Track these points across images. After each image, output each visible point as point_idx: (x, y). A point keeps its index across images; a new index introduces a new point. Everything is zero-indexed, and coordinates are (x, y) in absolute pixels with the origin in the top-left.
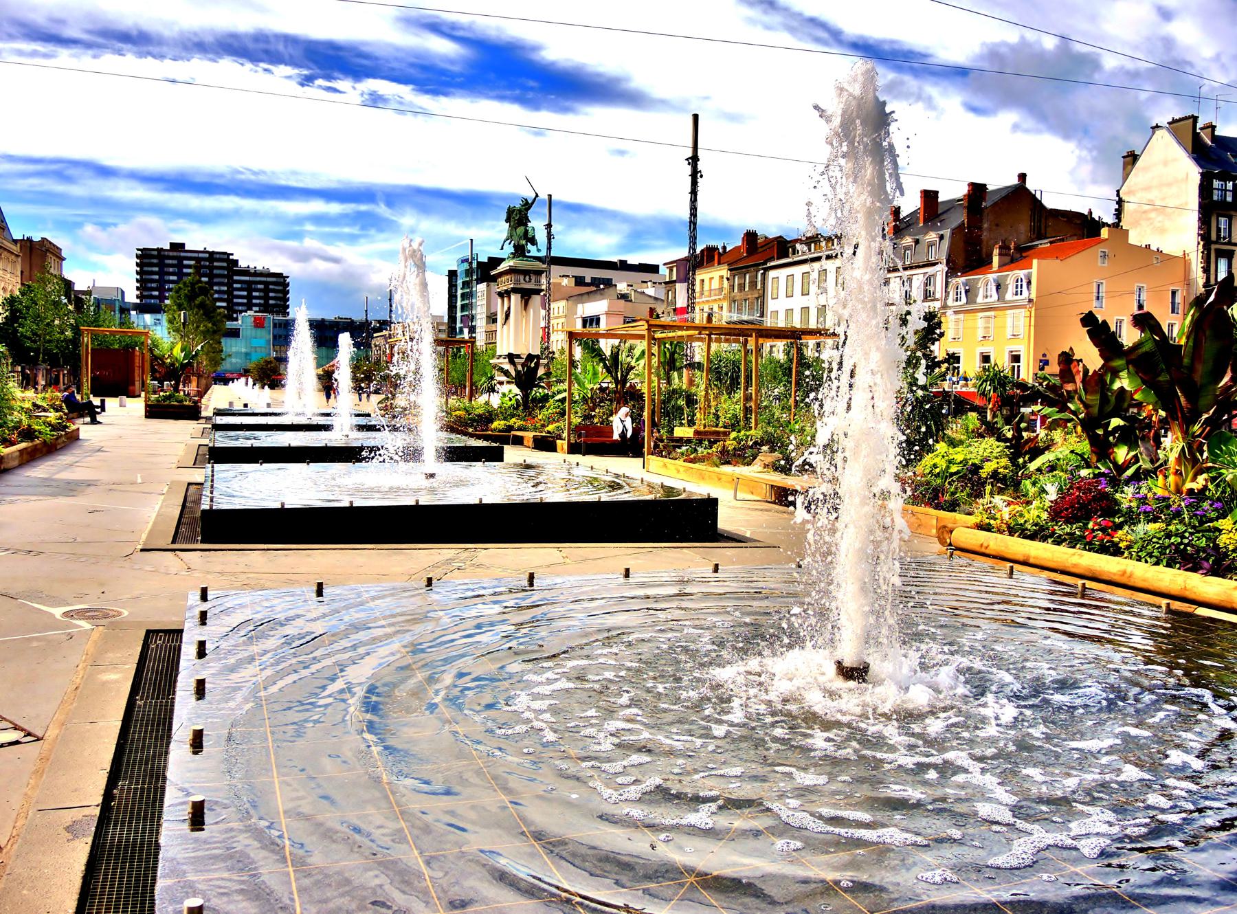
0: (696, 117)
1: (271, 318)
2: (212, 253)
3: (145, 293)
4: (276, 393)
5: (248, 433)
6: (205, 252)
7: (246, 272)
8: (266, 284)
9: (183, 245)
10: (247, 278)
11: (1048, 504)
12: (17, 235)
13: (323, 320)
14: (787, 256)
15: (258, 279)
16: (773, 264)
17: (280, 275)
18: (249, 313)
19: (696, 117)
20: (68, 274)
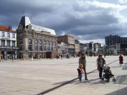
2: (115, 36)
7: (121, 38)
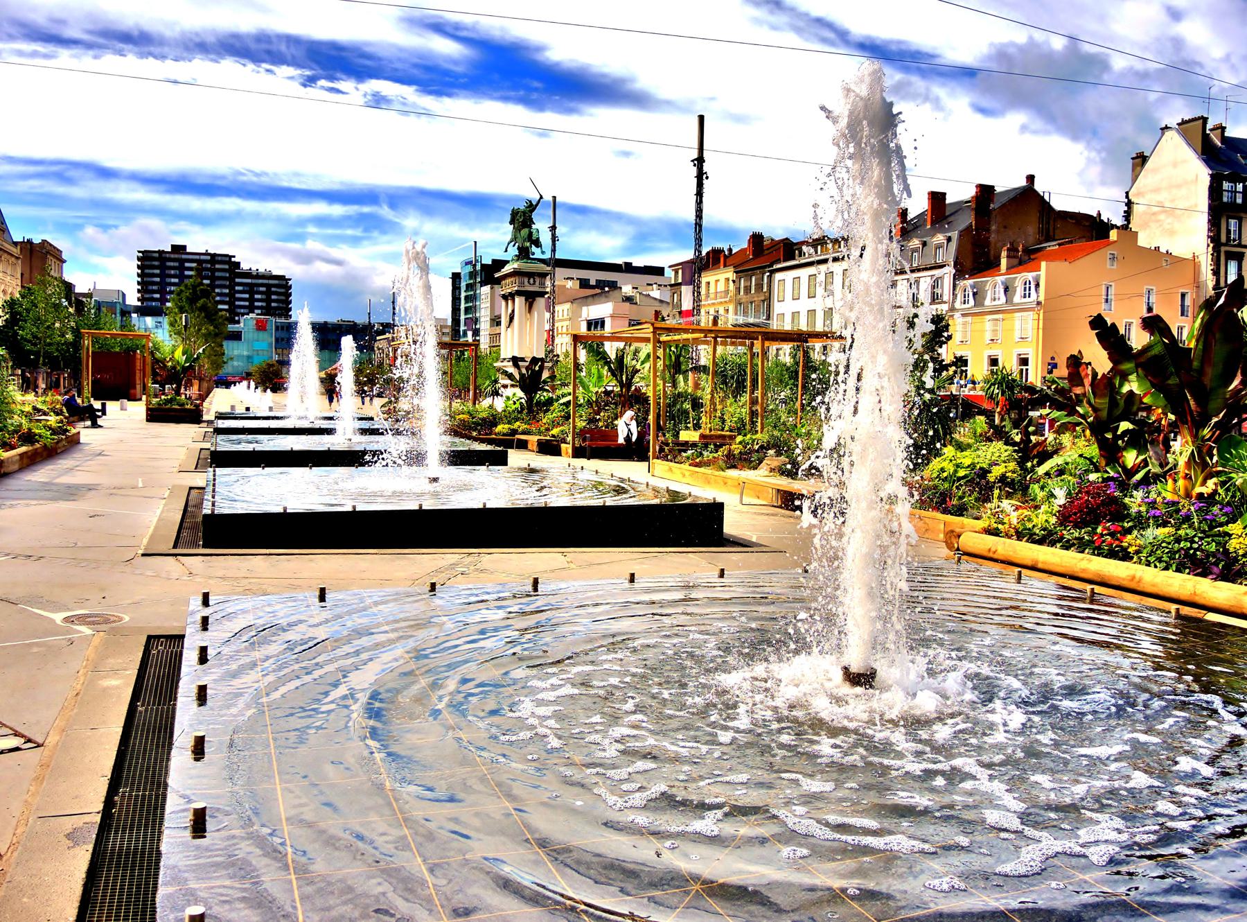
0: (701, 118)
1: (273, 321)
2: (214, 256)
3: (147, 296)
4: (278, 397)
5: (250, 437)
6: (206, 254)
7: (248, 274)
8: (268, 286)
9: (184, 247)
10: (249, 281)
11: (1056, 508)
12: (17, 237)
13: (326, 323)
14: (793, 258)
15: (260, 281)
16: (779, 266)
17: (282, 278)
18: (251, 315)
19: (701, 118)
20: (68, 276)
